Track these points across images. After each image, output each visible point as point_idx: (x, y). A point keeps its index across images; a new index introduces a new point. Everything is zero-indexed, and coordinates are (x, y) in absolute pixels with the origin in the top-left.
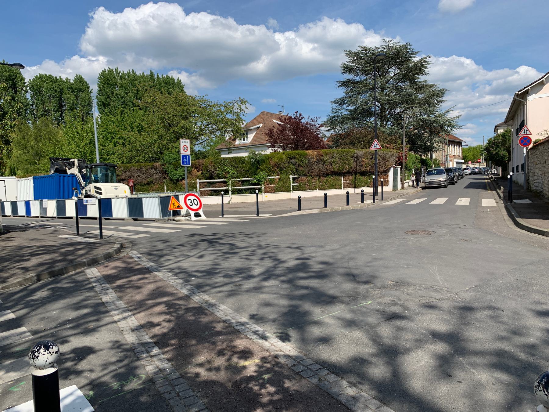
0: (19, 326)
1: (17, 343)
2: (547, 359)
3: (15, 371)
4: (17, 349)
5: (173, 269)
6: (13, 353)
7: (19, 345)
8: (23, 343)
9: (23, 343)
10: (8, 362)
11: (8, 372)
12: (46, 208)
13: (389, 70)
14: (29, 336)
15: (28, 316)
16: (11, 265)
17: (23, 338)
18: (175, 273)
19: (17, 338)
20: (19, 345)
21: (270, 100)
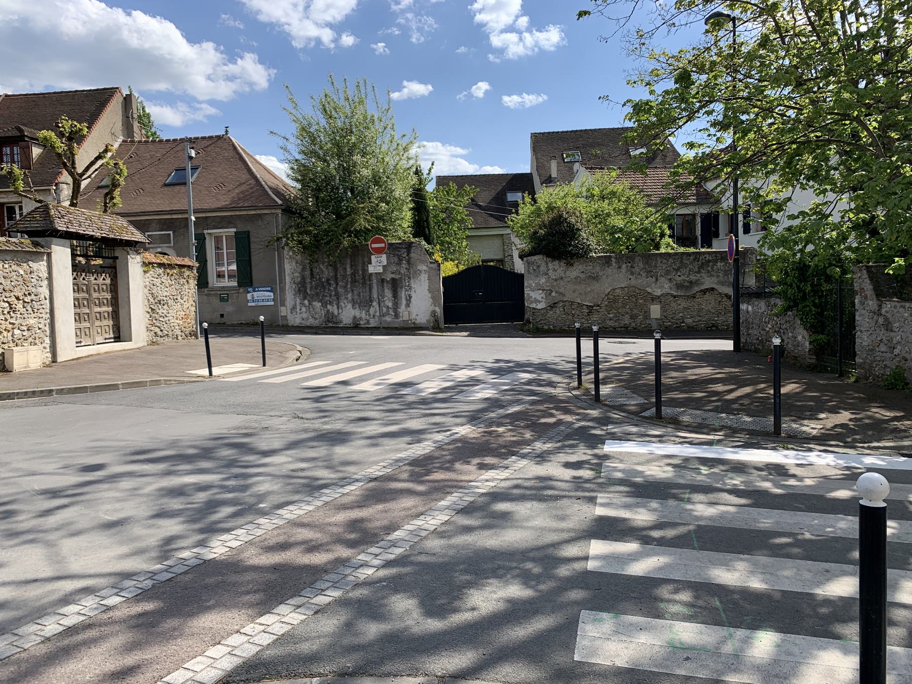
0: (601, 520)
1: (619, 494)
2: (911, 503)
3: (636, 470)
4: (622, 488)
5: (155, 574)
6: (628, 486)
7: (617, 492)
8: (613, 492)
9: (613, 492)
10: (638, 480)
11: (643, 472)
12: (249, 232)
13: (783, 390)
14: (601, 497)
15: (573, 534)
16: (76, 456)
17: (608, 498)
18: (223, 463)
19: (615, 501)
20: (617, 492)
21: (821, 382)
